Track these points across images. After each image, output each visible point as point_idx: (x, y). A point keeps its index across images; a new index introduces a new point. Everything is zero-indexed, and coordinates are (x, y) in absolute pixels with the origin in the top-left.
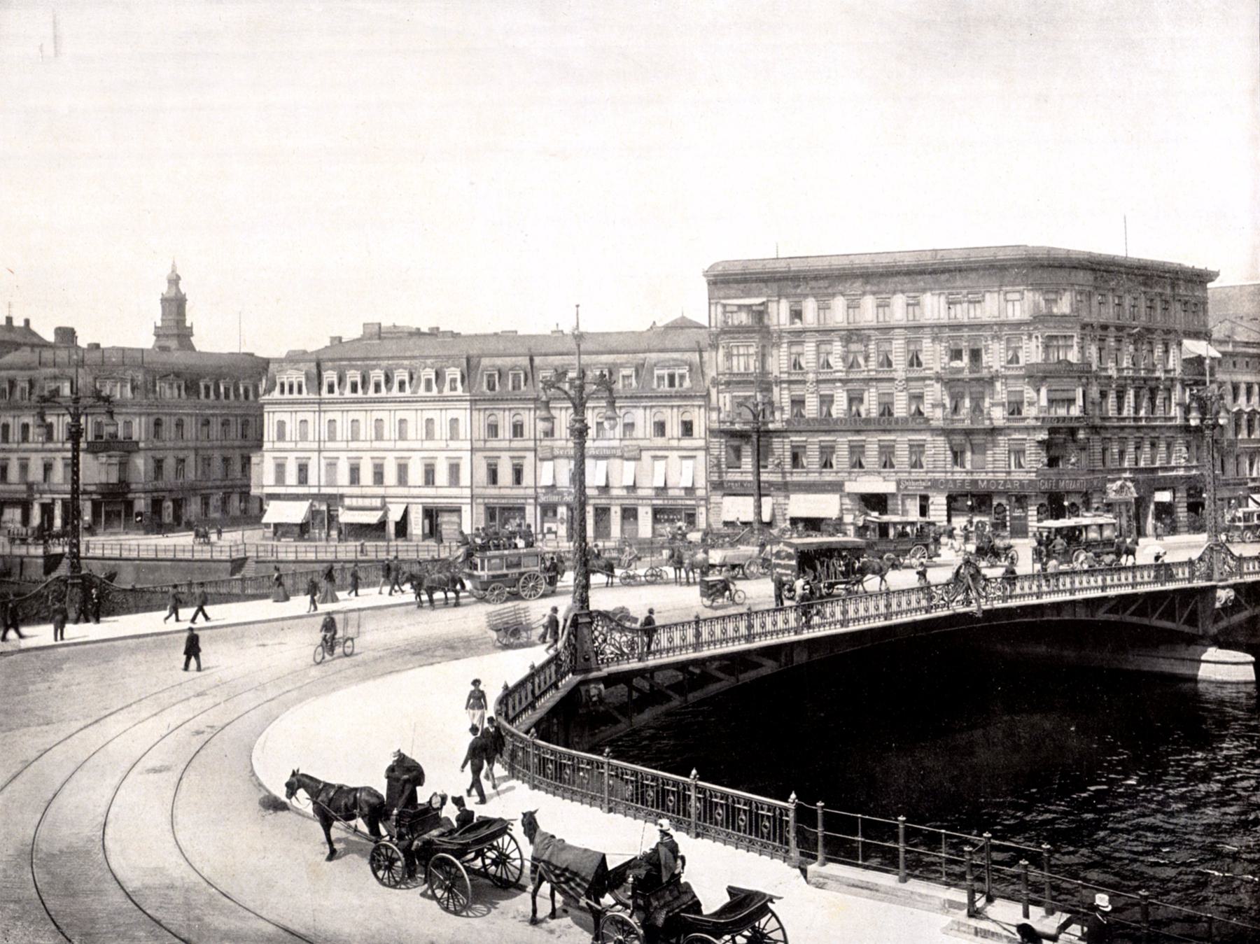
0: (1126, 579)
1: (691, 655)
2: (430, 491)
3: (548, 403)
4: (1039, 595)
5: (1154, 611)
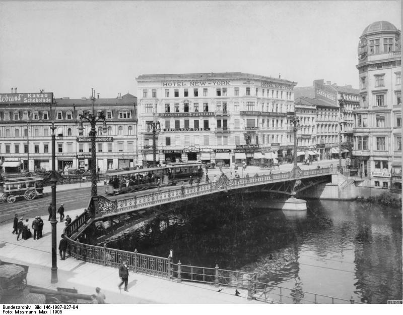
0: (208, 188)
1: (133, 209)
2: (37, 155)
3: (82, 123)
4: (245, 185)
5: (270, 188)
